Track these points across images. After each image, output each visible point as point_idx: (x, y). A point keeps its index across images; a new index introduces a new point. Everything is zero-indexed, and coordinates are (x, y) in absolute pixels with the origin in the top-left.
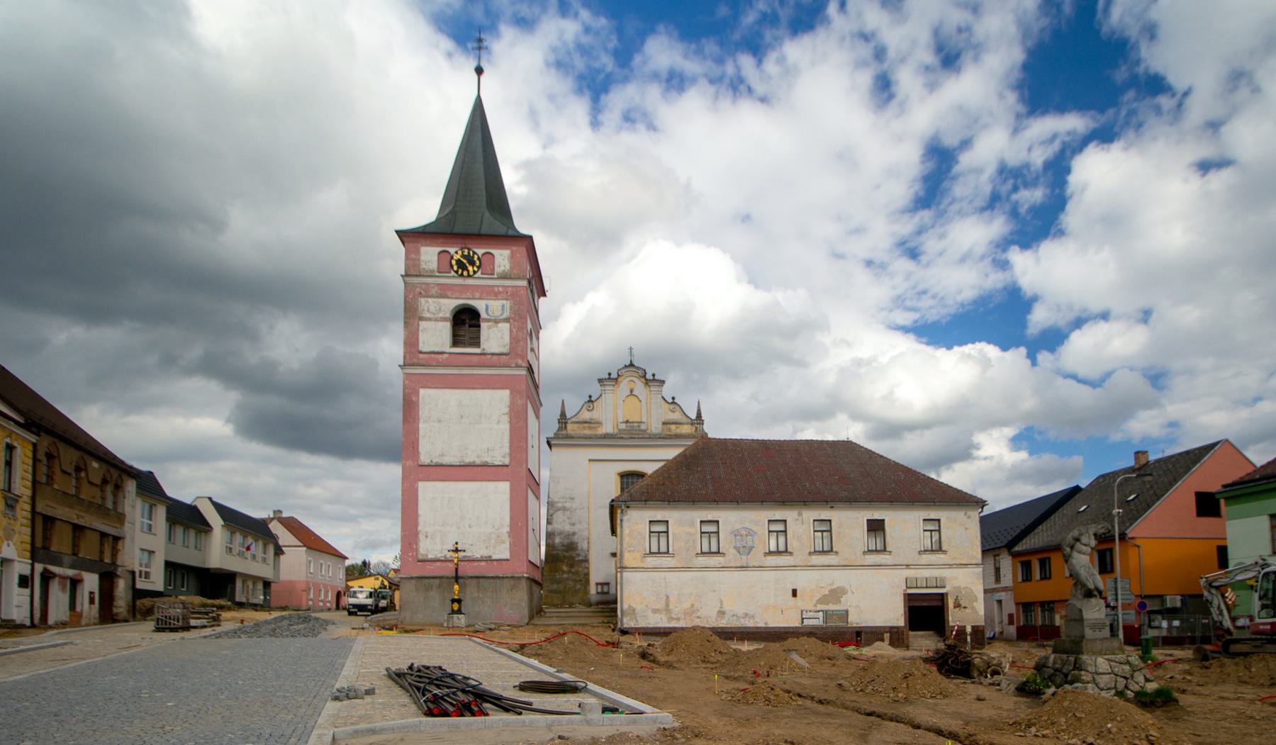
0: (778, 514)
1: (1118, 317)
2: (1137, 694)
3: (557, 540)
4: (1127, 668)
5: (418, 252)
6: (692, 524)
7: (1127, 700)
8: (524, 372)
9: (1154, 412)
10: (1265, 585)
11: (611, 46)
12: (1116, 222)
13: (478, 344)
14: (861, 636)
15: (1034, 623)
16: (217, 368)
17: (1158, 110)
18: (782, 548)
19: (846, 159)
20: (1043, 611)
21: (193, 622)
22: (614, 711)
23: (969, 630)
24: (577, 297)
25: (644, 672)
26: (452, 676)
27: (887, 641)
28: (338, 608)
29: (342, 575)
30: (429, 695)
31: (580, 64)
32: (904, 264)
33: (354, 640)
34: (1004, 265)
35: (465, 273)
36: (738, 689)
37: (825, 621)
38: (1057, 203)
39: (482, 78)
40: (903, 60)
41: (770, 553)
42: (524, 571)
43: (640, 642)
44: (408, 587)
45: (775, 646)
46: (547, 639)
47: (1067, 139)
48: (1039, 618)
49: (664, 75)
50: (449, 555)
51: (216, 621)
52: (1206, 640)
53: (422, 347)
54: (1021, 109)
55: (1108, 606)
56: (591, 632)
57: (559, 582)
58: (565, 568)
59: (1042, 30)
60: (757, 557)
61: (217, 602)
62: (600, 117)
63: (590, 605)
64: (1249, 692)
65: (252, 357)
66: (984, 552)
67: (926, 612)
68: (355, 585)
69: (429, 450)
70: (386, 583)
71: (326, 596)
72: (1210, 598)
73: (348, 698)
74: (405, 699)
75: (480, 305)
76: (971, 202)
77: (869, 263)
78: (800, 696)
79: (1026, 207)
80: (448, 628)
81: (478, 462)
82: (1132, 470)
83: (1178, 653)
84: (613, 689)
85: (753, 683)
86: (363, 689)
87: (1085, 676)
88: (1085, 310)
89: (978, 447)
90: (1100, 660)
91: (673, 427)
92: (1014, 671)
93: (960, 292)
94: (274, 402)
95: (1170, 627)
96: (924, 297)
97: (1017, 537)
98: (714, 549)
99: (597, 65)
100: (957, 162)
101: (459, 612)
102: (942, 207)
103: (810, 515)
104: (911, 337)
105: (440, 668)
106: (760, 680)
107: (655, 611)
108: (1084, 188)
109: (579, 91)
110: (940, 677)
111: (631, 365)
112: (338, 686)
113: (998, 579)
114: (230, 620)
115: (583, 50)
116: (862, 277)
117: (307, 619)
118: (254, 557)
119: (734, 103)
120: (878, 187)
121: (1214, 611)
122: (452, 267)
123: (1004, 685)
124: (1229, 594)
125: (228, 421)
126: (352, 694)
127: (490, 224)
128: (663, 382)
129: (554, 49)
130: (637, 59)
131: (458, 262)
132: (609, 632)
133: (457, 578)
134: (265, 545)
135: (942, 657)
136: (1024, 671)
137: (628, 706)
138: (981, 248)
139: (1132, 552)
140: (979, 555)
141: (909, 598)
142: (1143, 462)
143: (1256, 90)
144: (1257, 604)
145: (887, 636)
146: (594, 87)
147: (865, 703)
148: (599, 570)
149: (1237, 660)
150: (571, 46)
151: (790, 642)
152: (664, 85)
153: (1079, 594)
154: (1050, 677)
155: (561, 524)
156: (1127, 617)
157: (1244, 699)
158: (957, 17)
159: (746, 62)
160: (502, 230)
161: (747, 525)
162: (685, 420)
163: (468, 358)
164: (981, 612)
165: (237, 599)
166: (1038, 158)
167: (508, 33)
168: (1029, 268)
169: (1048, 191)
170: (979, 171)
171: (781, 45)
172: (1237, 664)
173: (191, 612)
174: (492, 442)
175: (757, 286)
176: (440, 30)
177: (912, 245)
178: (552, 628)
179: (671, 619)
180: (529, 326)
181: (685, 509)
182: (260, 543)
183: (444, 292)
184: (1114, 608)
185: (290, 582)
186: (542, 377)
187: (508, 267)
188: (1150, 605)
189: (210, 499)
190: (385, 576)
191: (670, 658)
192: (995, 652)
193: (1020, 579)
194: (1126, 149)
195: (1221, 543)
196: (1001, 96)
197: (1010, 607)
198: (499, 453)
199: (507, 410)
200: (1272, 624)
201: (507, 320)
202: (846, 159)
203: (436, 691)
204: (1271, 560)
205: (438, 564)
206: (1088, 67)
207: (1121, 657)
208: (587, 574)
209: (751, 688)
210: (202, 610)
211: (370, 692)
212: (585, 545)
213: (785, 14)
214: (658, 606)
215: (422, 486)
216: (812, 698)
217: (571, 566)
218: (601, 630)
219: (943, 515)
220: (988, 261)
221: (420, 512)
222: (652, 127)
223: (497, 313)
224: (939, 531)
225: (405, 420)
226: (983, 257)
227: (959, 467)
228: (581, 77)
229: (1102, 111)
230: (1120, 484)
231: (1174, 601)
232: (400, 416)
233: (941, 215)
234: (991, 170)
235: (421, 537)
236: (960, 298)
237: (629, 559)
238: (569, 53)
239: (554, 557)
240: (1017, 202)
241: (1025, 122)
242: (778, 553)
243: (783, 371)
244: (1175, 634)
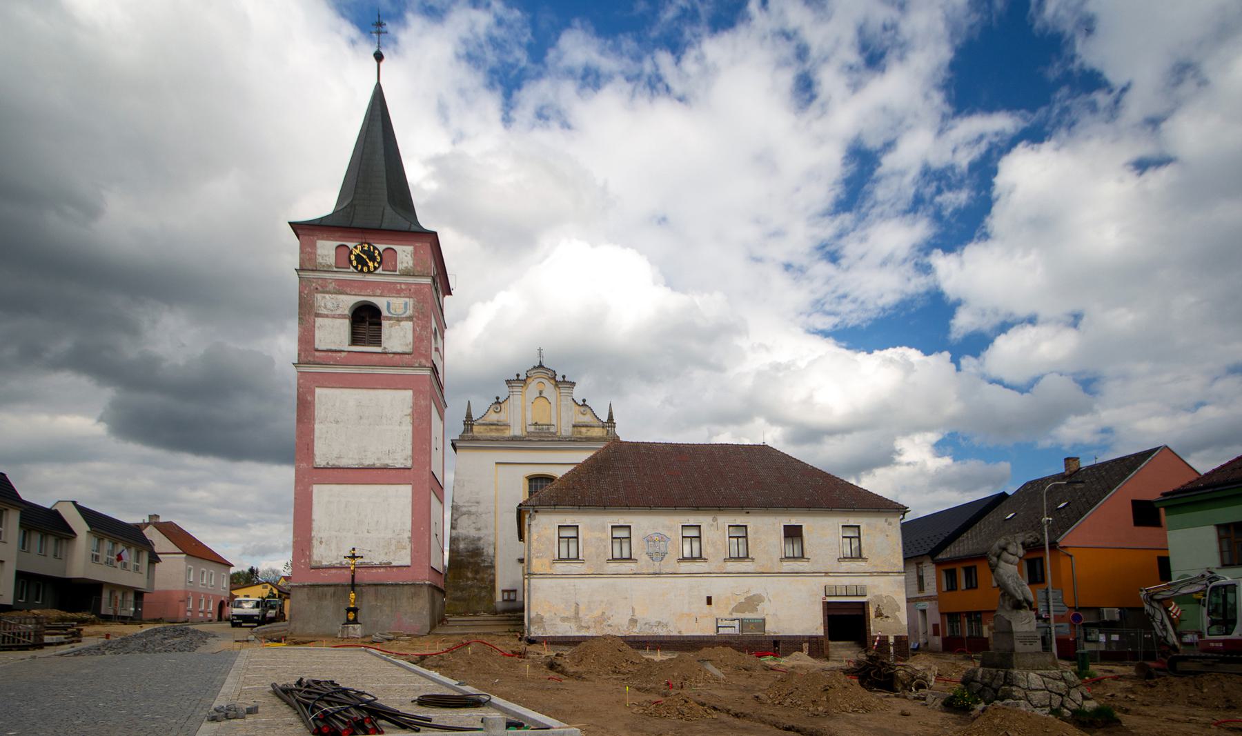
0: (692, 520)
1: (1047, 322)
2: (1074, 712)
3: (462, 546)
4: (1062, 684)
5: (314, 246)
6: (604, 529)
7: (1064, 719)
8: (428, 372)
9: (1087, 418)
10: (1214, 599)
11: (525, 40)
12: (1044, 224)
13: (378, 342)
14: (781, 645)
15: (960, 634)
16: (92, 363)
17: (1093, 108)
18: (696, 554)
19: (765, 161)
20: (970, 622)
21: (47, 639)
22: (519, 726)
23: (891, 640)
24: (488, 297)
25: (551, 684)
26: (345, 691)
27: (806, 652)
28: (220, 619)
29: (226, 583)
30: (318, 713)
31: (491, 57)
32: (823, 268)
33: (237, 654)
34: (927, 269)
35: (365, 269)
36: (650, 702)
37: (741, 630)
38: (983, 204)
39: (382, 64)
40: (825, 60)
41: (684, 559)
42: (425, 578)
43: (548, 652)
44: (299, 596)
45: (690, 655)
46: (449, 650)
47: (995, 140)
48: (965, 630)
49: (580, 72)
50: (345, 561)
51: (77, 636)
52: (1149, 656)
53: (318, 345)
54: (947, 109)
55: (1038, 617)
56: (497, 642)
57: (462, 589)
58: (470, 575)
59: (971, 27)
60: (670, 564)
61: (79, 615)
62: (512, 114)
63: (495, 613)
64: (1202, 715)
65: (130, 350)
66: (906, 560)
67: (846, 620)
68: (240, 594)
69: (324, 453)
70: (275, 592)
71: (207, 606)
72: (1151, 611)
73: (227, 717)
74: (291, 717)
75: (381, 302)
76: (893, 205)
77: (788, 267)
78: (715, 708)
79: (950, 210)
80: (343, 639)
81: (378, 464)
82: (1061, 477)
83: (1119, 669)
84: (518, 703)
85: (666, 695)
86: (245, 707)
87: (1017, 692)
88: (1011, 314)
89: (899, 453)
90: (1032, 675)
91: (584, 430)
92: (940, 685)
93: (881, 296)
94: (154, 401)
95: (1108, 641)
96: (845, 301)
97: (939, 543)
98: (626, 555)
99: (511, 60)
100: (880, 165)
101: (355, 621)
102: (863, 210)
103: (725, 520)
104: (831, 341)
105: (332, 682)
106: (673, 692)
107: (564, 619)
108: (1012, 190)
109: (490, 86)
110: (862, 691)
111: (541, 366)
112: (216, 705)
113: (921, 588)
114: (93, 635)
115: (494, 42)
116: (780, 281)
117: (184, 632)
118: (125, 565)
119: (651, 102)
120: (798, 190)
121: (1157, 626)
122: (351, 262)
123: (930, 699)
124: (1174, 608)
125: (100, 420)
126: (231, 713)
127: (391, 218)
128: (574, 384)
129: (465, 42)
130: (552, 54)
131: (358, 257)
132: (516, 641)
133: (353, 586)
134: (138, 553)
135: (864, 669)
136: (951, 685)
137: (534, 721)
138: (902, 253)
139: (1064, 562)
140: (901, 564)
141: (829, 607)
142: (1073, 468)
143: (1203, 83)
144: (1205, 620)
145: (806, 646)
146: (507, 82)
147: (784, 717)
148: (505, 577)
149: (1186, 679)
150: (483, 38)
151: (705, 652)
152: (580, 81)
153: (1007, 605)
154: (979, 692)
155: (467, 529)
156: (1060, 629)
157: (1197, 722)
158: (883, 14)
159: (664, 59)
160: (404, 225)
161: (661, 531)
162: (595, 422)
163: (369, 357)
164: (904, 621)
165: (103, 612)
166: (964, 160)
167: (415, 21)
168: (952, 272)
169: (973, 194)
170: (902, 173)
171: (700, 42)
172: (1186, 684)
173: (44, 626)
174: (395, 446)
175: (673, 289)
176: (343, 15)
177: (832, 248)
178: (456, 638)
179: (581, 627)
180: (434, 325)
181: (595, 513)
182: (133, 550)
183: (342, 288)
184: (1046, 620)
185: (167, 592)
186: (447, 378)
187: (411, 263)
188: (1085, 617)
189: (74, 503)
190: (275, 585)
191: (581, 669)
192: (919, 665)
193: (944, 588)
194: (1057, 149)
195: (1162, 554)
196: (926, 97)
197: (935, 617)
198: (401, 455)
199: (409, 411)
200: (1223, 641)
201: (410, 318)
202: (765, 161)
203: (327, 708)
204: (1219, 573)
205: (334, 571)
206: (1020, 66)
207: (1054, 672)
208: (493, 581)
209: (663, 700)
210: (60, 624)
211: (252, 711)
212: (491, 551)
213: (705, 10)
214: (567, 614)
215: (316, 489)
216: (728, 712)
217: (477, 572)
218: (507, 640)
219: (864, 522)
220: (909, 266)
221: (314, 517)
222: (566, 125)
223: (400, 311)
224: (859, 537)
225: (299, 420)
226: (905, 261)
227: (880, 472)
228: (493, 71)
229: (1033, 109)
230: (1050, 492)
231: (1112, 614)
232: (294, 416)
233: (862, 218)
234: (914, 172)
235: (315, 543)
236: (881, 303)
237: (537, 565)
238: (481, 46)
239: (457, 562)
240: (941, 205)
241: (951, 123)
242: (692, 559)
243: (699, 375)
244: (1114, 648)
